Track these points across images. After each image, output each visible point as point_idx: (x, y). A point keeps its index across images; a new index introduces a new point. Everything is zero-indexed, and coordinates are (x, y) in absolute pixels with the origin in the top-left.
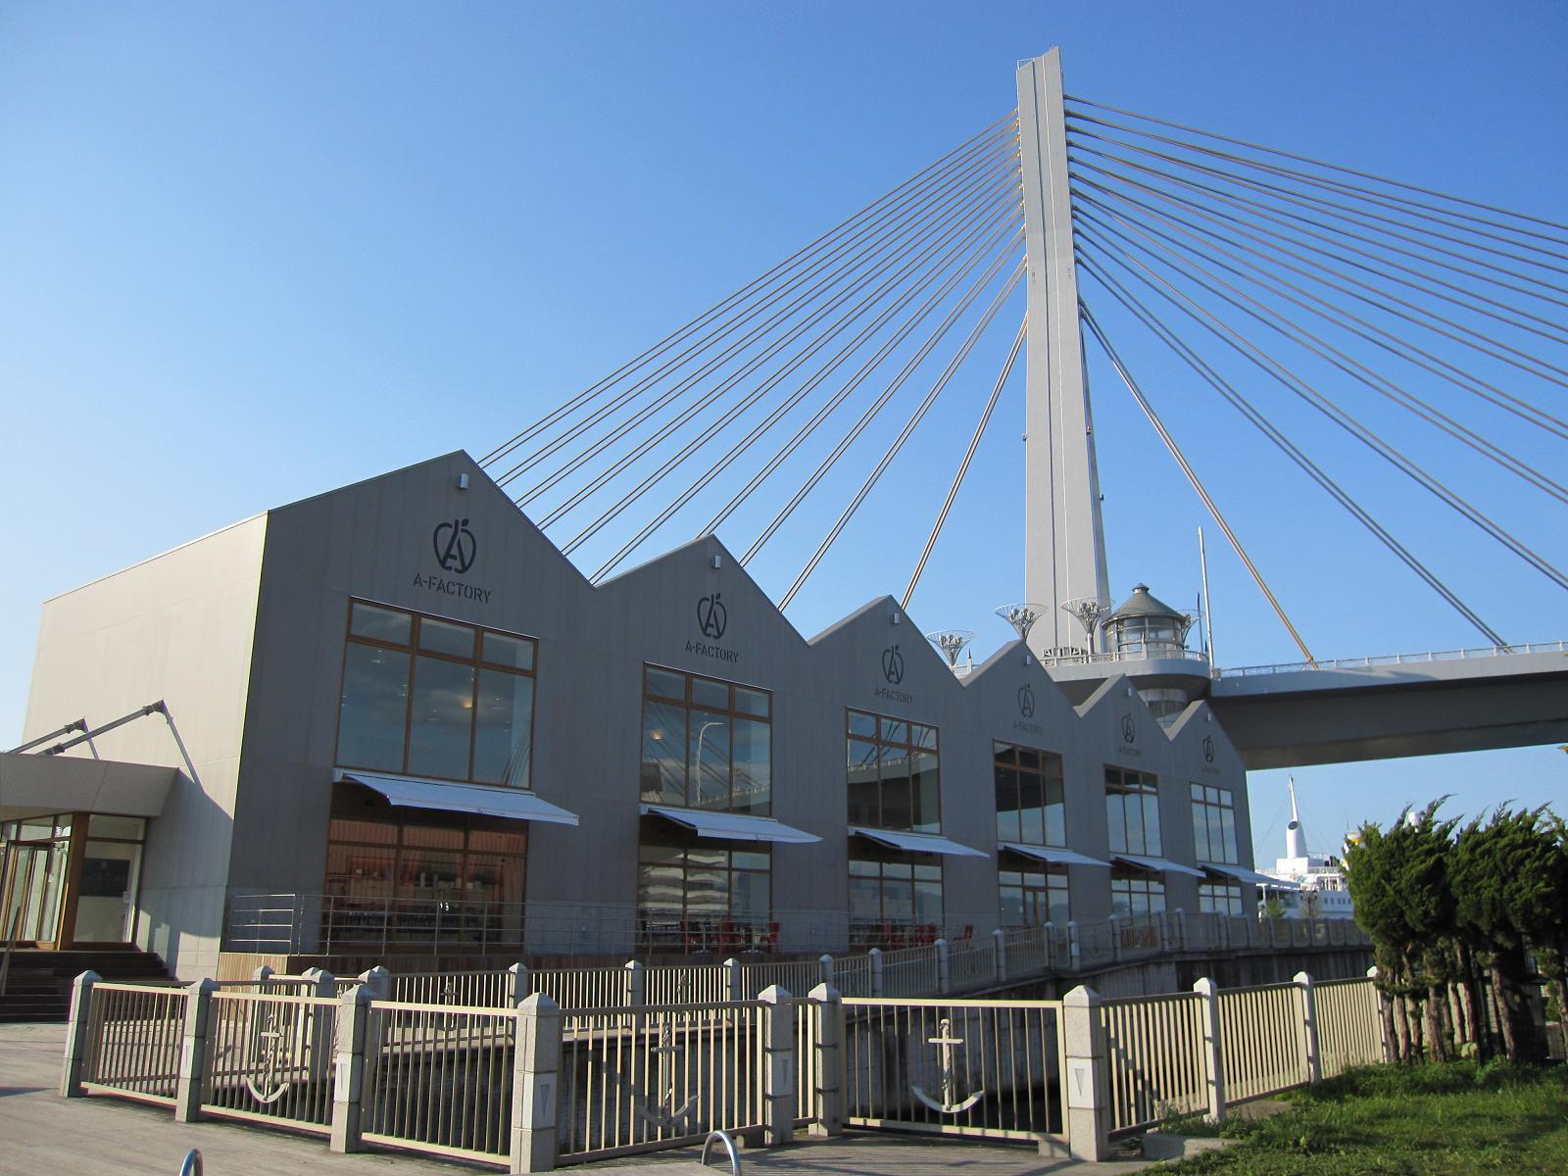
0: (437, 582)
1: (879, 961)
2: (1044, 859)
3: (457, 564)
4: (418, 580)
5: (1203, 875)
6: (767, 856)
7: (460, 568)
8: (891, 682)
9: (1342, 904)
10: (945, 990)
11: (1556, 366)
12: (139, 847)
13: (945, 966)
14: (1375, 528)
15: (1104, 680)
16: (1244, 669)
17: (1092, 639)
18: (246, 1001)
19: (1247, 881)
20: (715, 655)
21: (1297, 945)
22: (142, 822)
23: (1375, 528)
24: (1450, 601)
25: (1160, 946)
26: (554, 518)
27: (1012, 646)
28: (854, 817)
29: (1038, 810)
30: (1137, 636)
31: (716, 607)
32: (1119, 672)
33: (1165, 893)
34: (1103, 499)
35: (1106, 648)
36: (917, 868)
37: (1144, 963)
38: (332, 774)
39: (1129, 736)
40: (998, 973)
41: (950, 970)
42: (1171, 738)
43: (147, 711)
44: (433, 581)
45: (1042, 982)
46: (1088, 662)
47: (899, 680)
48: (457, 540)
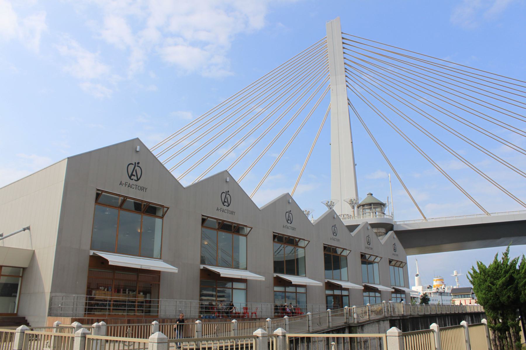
0: (222, 209)
1: (287, 320)
2: (341, 285)
3: (135, 178)
4: (121, 183)
5: (393, 290)
6: (405, 295)
7: (227, 205)
8: (334, 235)
9: (433, 301)
10: (311, 331)
11: (508, 128)
12: (20, 278)
13: (310, 322)
14: (466, 194)
15: (359, 225)
16: (404, 221)
17: (354, 211)
18: (42, 335)
19: (408, 292)
20: (135, 188)
21: (426, 313)
22: (22, 269)
23: (466, 194)
24: (480, 205)
25: (384, 314)
26: (168, 160)
27: (284, 195)
28: (275, 271)
29: (340, 270)
30: (369, 210)
31: (227, 195)
32: (365, 221)
33: (246, 289)
34: (356, 165)
35: (358, 214)
36: (370, 293)
37: (378, 321)
38: (89, 252)
39: (369, 243)
40: (329, 324)
41: (312, 323)
42: (383, 244)
43: (24, 230)
44: (221, 209)
45: (344, 327)
46: (353, 219)
47: (291, 223)
48: (135, 170)
